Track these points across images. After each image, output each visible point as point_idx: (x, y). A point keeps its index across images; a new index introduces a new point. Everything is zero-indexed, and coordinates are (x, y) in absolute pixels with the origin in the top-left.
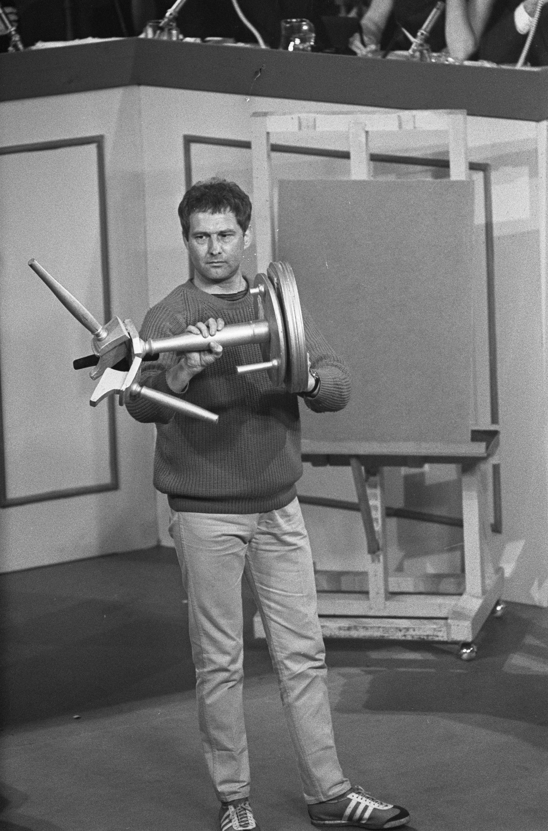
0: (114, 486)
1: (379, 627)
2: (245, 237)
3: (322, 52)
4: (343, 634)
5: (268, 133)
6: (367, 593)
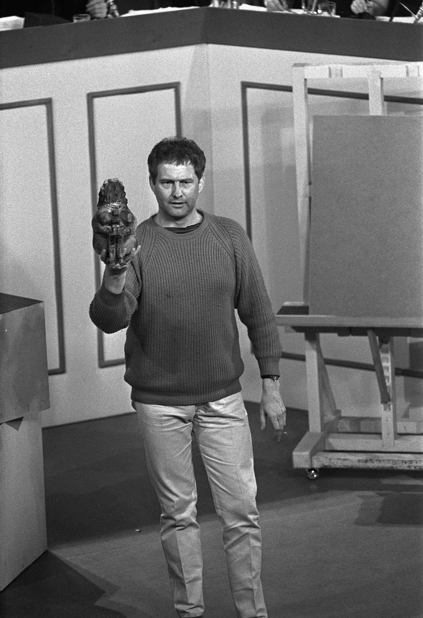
0: (91, 97)
1: (390, 460)
2: (200, 184)
3: (348, 17)
4: (362, 465)
5: (306, 80)
6: (380, 434)
